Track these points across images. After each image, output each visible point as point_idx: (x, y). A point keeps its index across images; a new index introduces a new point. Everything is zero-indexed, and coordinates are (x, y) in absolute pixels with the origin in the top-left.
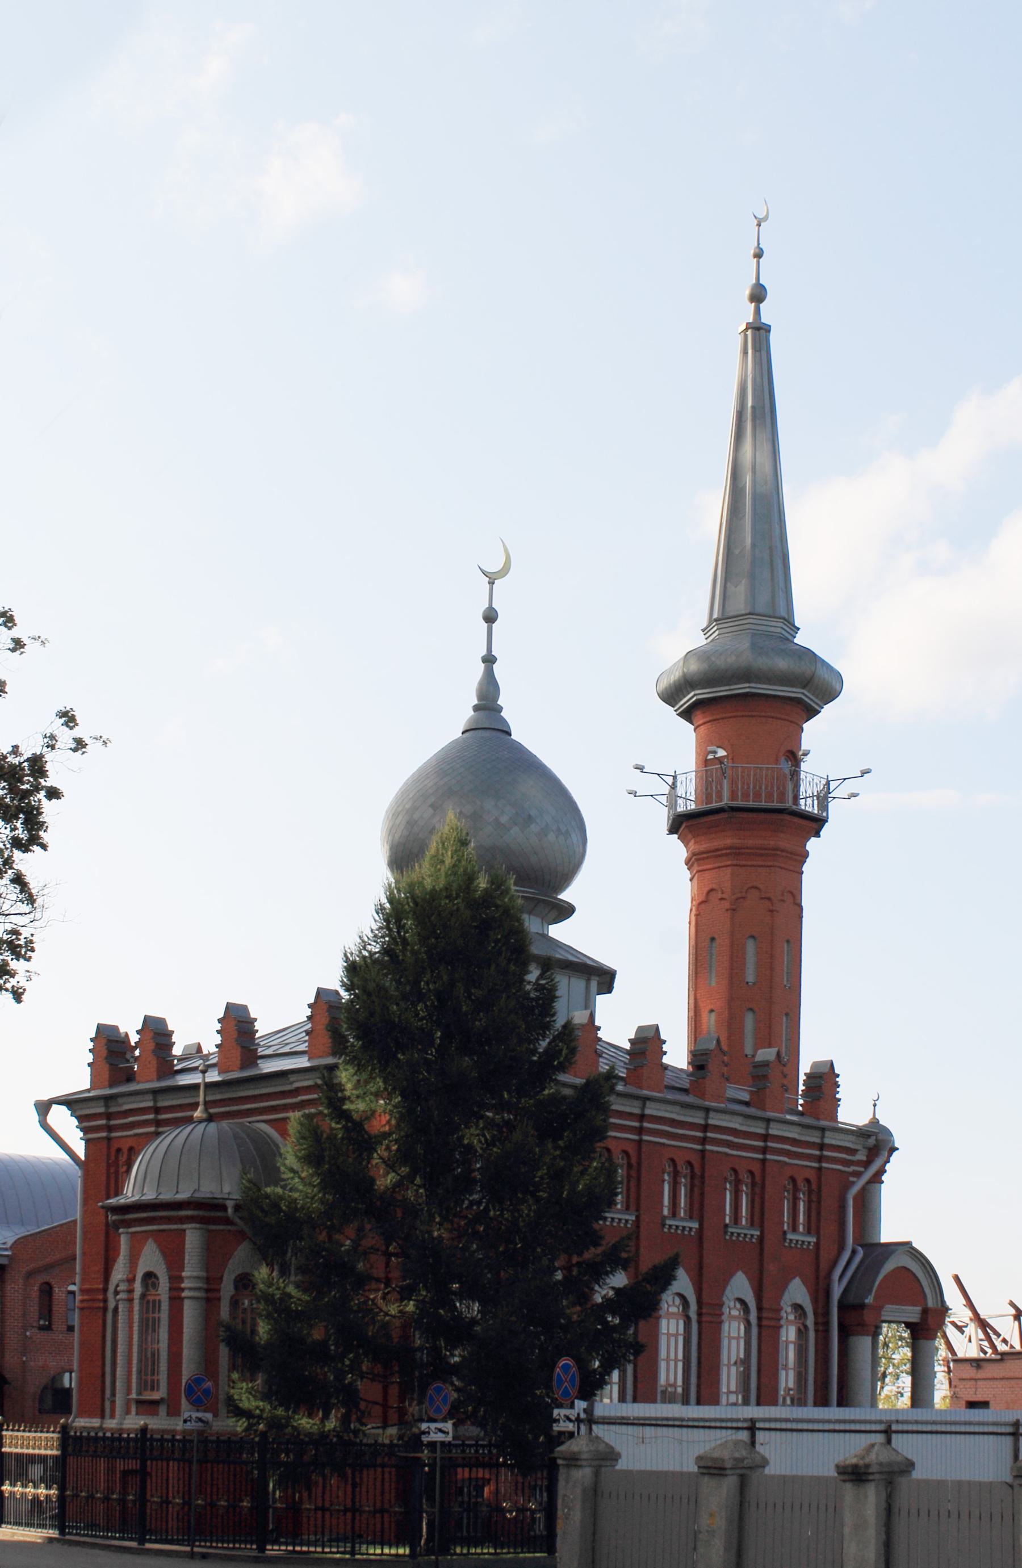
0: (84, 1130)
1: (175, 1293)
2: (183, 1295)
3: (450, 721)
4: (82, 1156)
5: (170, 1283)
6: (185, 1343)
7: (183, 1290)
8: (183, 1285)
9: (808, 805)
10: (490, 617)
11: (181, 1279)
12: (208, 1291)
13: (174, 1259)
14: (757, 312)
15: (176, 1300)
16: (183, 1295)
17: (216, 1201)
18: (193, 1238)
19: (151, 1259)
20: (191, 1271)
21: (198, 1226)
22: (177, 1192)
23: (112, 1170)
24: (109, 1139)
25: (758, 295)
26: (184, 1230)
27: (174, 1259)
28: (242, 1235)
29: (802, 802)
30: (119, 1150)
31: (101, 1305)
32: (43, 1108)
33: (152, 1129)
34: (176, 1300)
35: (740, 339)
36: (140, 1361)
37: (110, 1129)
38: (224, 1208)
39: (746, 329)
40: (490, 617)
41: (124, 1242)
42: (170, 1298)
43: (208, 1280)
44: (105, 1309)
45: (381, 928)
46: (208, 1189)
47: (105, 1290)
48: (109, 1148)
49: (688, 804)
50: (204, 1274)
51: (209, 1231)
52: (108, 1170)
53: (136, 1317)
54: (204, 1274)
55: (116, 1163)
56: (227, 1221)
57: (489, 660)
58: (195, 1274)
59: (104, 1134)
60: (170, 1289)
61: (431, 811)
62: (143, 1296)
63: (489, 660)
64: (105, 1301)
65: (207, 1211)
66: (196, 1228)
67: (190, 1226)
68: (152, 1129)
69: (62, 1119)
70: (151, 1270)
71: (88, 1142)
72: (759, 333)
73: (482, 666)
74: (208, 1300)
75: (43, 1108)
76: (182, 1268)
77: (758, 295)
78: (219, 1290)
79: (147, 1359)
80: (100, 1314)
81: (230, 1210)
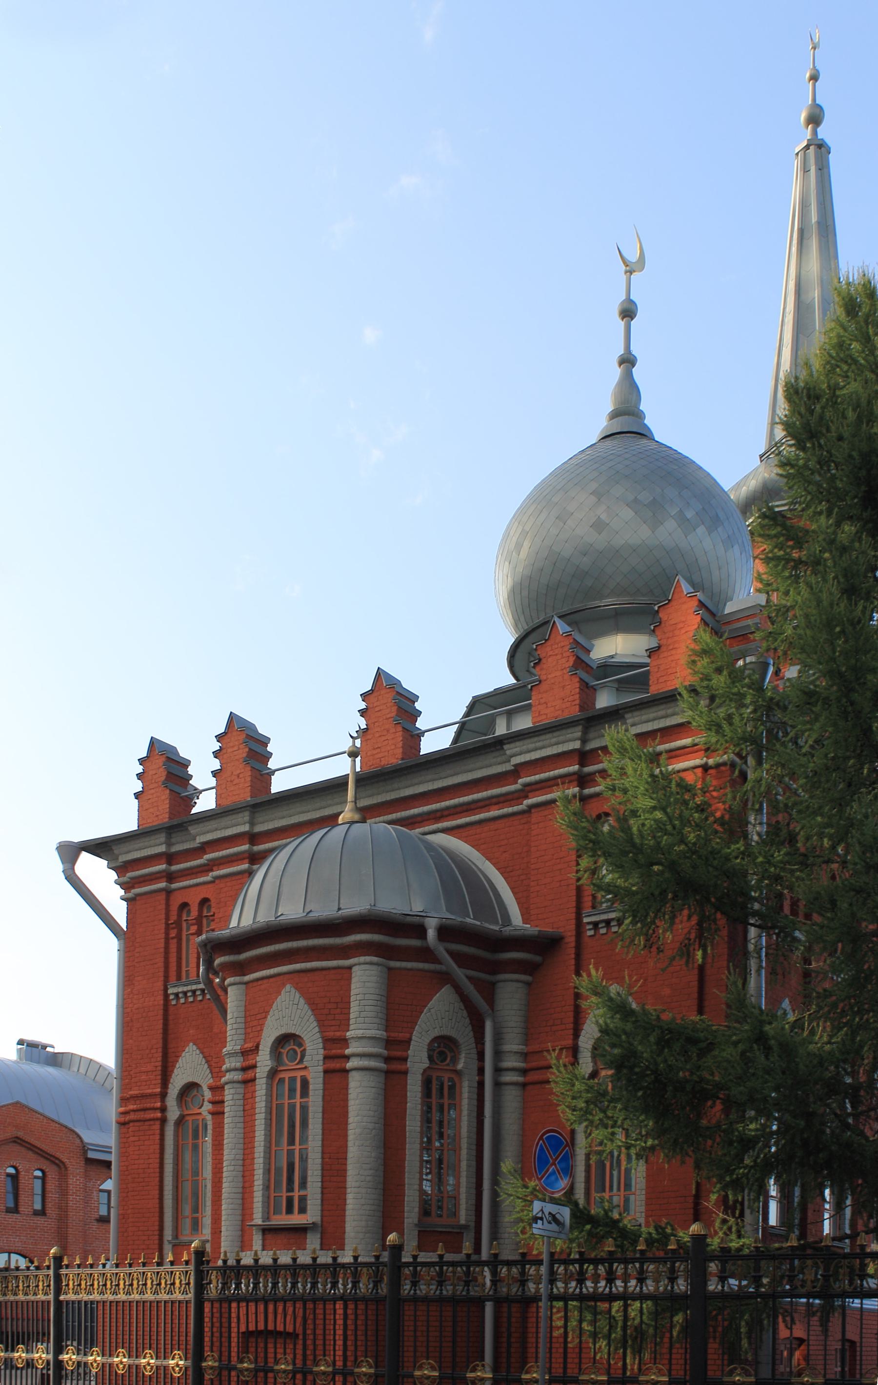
0: (125, 886)
1: (335, 1065)
2: (349, 1065)
3: (592, 422)
4: (123, 924)
5: (324, 1048)
6: (351, 1137)
7: (347, 1058)
8: (347, 1052)
10: (628, 313)
11: (344, 1042)
12: (387, 1060)
13: (332, 1013)
14: (815, 133)
15: (336, 1072)
16: (349, 1065)
17: (409, 919)
18: (364, 980)
19: (289, 1012)
20: (363, 1026)
21: (375, 959)
22: (339, 909)
23: (173, 933)
24: (168, 892)
25: (815, 119)
26: (350, 968)
27: (332, 1013)
28: (445, 978)
30: (184, 906)
31: (159, 1115)
32: (70, 852)
33: (245, 866)
34: (336, 1072)
35: (796, 163)
36: (267, 1171)
37: (171, 877)
38: (419, 930)
39: (807, 147)
40: (628, 313)
41: (234, 998)
42: (326, 1072)
43: (389, 1043)
44: (163, 1121)
45: (786, 416)
46: (391, 904)
47: (163, 1095)
48: (168, 905)
50: (381, 1034)
51: (390, 969)
52: (167, 934)
53: (261, 1105)
54: (381, 1034)
55: (178, 924)
56: (426, 954)
57: (628, 361)
58: (369, 1033)
59: (163, 885)
60: (326, 1058)
61: (593, 499)
62: (273, 1073)
63: (628, 361)
64: (163, 1109)
65: (388, 934)
66: (371, 963)
67: (362, 959)
68: (245, 866)
69: (96, 872)
70: (283, 1031)
71: (130, 901)
72: (819, 148)
73: (617, 372)
74: (388, 1073)
75: (70, 852)
76: (345, 1024)
77: (815, 119)
78: (405, 1059)
79: (278, 1171)
80: (157, 1126)
81: (431, 934)
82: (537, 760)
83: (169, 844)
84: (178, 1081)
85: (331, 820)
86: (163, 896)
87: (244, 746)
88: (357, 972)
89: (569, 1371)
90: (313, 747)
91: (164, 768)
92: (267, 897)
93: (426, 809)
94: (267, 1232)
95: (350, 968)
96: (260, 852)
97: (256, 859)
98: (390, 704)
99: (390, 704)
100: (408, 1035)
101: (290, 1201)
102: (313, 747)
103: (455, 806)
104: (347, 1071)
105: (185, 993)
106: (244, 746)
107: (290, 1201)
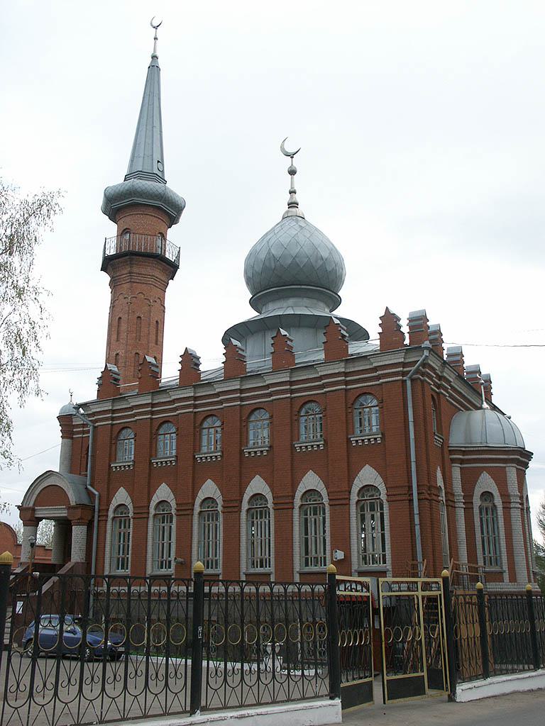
9: (170, 256)
29: (167, 253)
49: (112, 251)
83: (113, 406)
86: (289, 400)
93: (393, 370)
95: (505, 467)
96: (115, 417)
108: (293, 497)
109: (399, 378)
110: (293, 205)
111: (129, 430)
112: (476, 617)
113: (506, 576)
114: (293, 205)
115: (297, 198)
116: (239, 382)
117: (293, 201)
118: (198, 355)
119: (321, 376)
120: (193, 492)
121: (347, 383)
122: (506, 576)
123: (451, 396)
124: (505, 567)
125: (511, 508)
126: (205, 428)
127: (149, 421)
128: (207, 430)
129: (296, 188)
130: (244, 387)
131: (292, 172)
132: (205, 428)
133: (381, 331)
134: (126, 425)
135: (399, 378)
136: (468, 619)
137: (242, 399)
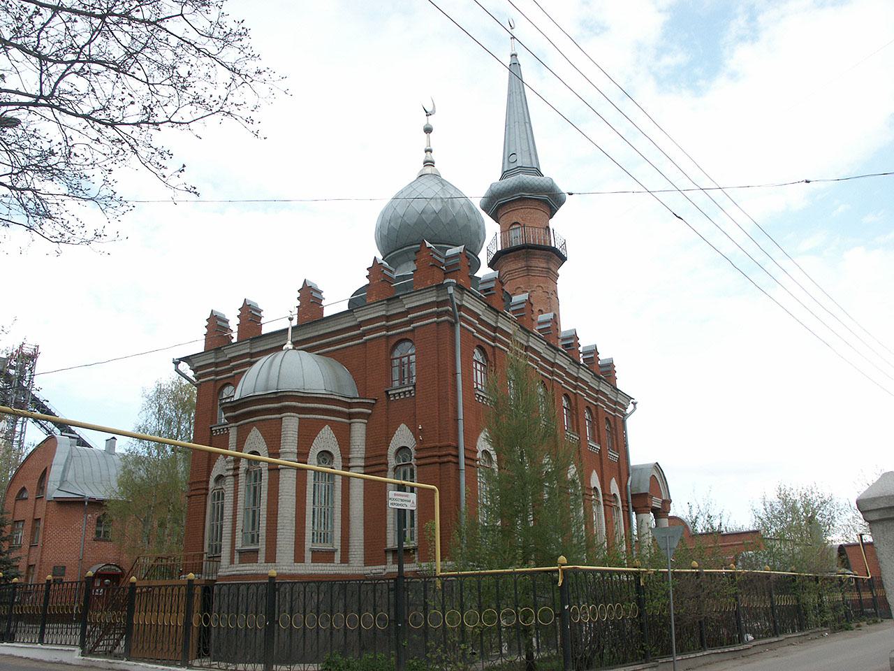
8: (350, 465)
26: (281, 418)
32: (176, 363)
75: (176, 363)
82: (368, 319)
84: (214, 474)
85: (280, 348)
86: (213, 382)
87: (250, 315)
88: (286, 422)
89: (395, 361)
90: (279, 314)
91: (216, 325)
92: (252, 382)
94: (501, 212)
95: (281, 418)
97: (251, 364)
98: (310, 297)
99: (310, 297)
100: (307, 451)
101: (207, 607)
102: (279, 314)
103: (340, 339)
104: (279, 470)
105: (219, 430)
106: (250, 315)
107: (207, 607)
108: (208, 482)
109: (433, 320)
110: (429, 163)
111: (408, 344)
112: (182, 607)
113: (338, 556)
114: (429, 163)
115: (434, 156)
116: (248, 345)
117: (429, 159)
118: (227, 318)
119: (197, 367)
120: (372, 473)
121: (217, 374)
122: (338, 556)
123: (479, 331)
124: (337, 544)
125: (279, 470)
126: (396, 359)
127: (434, 325)
128: (398, 360)
129: (432, 147)
130: (254, 351)
131: (428, 130)
132: (396, 359)
133: (335, 303)
134: (404, 336)
135: (433, 320)
136: (180, 608)
137: (388, 328)
